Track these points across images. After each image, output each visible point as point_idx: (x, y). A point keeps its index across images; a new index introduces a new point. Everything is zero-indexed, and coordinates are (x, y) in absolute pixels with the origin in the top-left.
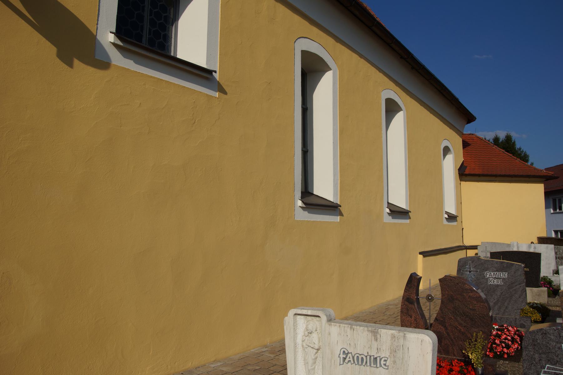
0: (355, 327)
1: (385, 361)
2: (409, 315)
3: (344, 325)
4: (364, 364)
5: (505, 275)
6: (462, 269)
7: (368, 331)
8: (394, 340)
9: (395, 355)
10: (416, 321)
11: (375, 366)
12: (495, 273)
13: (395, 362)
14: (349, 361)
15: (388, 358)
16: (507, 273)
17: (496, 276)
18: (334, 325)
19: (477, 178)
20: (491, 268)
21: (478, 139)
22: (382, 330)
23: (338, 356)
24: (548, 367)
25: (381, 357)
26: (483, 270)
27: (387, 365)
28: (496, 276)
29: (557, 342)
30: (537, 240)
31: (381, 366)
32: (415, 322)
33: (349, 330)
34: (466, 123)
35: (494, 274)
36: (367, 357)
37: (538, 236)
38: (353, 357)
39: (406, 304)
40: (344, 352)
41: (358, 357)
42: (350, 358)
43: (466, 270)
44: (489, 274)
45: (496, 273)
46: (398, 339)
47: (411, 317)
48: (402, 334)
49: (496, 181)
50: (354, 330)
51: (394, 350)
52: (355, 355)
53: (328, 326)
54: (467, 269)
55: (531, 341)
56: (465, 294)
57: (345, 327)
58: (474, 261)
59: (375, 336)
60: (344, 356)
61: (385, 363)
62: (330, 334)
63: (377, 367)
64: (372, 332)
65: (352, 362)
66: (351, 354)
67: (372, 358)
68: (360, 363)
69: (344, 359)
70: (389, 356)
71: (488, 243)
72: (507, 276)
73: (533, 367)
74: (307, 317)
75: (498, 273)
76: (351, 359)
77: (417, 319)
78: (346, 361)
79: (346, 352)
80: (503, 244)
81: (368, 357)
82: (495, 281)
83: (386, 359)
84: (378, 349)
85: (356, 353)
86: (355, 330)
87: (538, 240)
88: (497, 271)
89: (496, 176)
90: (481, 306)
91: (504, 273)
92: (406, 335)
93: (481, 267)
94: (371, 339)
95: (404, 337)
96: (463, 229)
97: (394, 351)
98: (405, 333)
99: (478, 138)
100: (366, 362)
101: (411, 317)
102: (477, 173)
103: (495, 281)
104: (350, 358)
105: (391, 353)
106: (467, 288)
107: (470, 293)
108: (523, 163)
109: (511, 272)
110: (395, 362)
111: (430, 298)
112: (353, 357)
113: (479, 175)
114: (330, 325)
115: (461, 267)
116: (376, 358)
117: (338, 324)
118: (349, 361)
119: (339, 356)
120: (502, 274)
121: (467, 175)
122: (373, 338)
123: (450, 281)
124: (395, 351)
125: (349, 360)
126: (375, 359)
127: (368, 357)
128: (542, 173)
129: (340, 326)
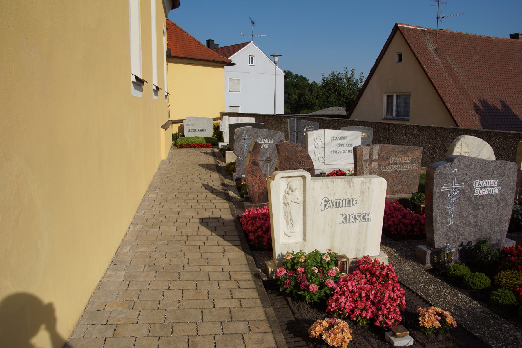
0: (335, 180)
1: (356, 200)
2: (254, 175)
3: (325, 180)
4: (340, 206)
5: (271, 141)
6: (239, 138)
7: (345, 181)
8: (363, 184)
9: (363, 195)
10: (261, 180)
11: (349, 206)
12: (265, 140)
13: (363, 200)
14: (329, 207)
15: (358, 198)
16: (273, 139)
17: (265, 142)
18: (317, 181)
19: (180, 60)
20: (262, 136)
21: (172, 24)
22: (354, 179)
23: (320, 204)
24: (445, 185)
25: (353, 199)
26: (256, 137)
27: (357, 203)
28: (265, 142)
29: (450, 171)
30: (219, 115)
31: (353, 204)
32: (260, 180)
33: (330, 182)
34: (171, 8)
35: (264, 140)
36: (344, 200)
37: (220, 112)
38: (332, 203)
39: (252, 166)
40: (325, 200)
41: (336, 202)
42: (330, 204)
43: (242, 138)
44: (260, 140)
45: (266, 140)
46: (366, 184)
47: (256, 177)
48: (368, 180)
49: (193, 64)
50: (334, 182)
51: (363, 192)
52: (334, 201)
53: (313, 182)
54: (243, 138)
55: (439, 173)
56: (298, 155)
57: (326, 181)
58: (249, 131)
59: (350, 184)
60: (326, 204)
61: (356, 202)
62: (314, 189)
63: (350, 206)
64: (347, 181)
65: (332, 206)
66: (331, 201)
67: (347, 200)
68: (338, 206)
69: (325, 205)
70: (359, 197)
71: (191, 117)
72: (273, 141)
73: (438, 187)
74: (289, 178)
75: (266, 140)
76: (331, 205)
77: (261, 178)
78: (327, 207)
79: (327, 200)
80: (204, 118)
81: (344, 201)
82: (264, 146)
83: (357, 199)
84: (351, 193)
85: (335, 199)
86: (334, 183)
87: (220, 115)
88: (266, 138)
89: (194, 59)
90: (309, 162)
91: (271, 139)
92: (371, 180)
93: (254, 136)
94: (347, 187)
95: (370, 181)
96: (169, 105)
97: (362, 193)
98: (370, 178)
99: (173, 23)
100: (342, 205)
101: (256, 177)
102: (181, 56)
103: (264, 146)
104: (330, 204)
105: (360, 195)
106: (299, 149)
107: (301, 153)
108: (209, 50)
109: (276, 138)
110: (363, 200)
111: (269, 160)
112: (332, 203)
113: (182, 58)
114: (314, 181)
115: (239, 136)
116: (350, 200)
117: (320, 180)
118: (329, 207)
119: (321, 204)
120: (269, 140)
121: (173, 57)
122: (348, 186)
123: (287, 145)
124: (364, 192)
125: (330, 205)
126: (349, 201)
127: (344, 201)
128: (224, 59)
129: (322, 181)
